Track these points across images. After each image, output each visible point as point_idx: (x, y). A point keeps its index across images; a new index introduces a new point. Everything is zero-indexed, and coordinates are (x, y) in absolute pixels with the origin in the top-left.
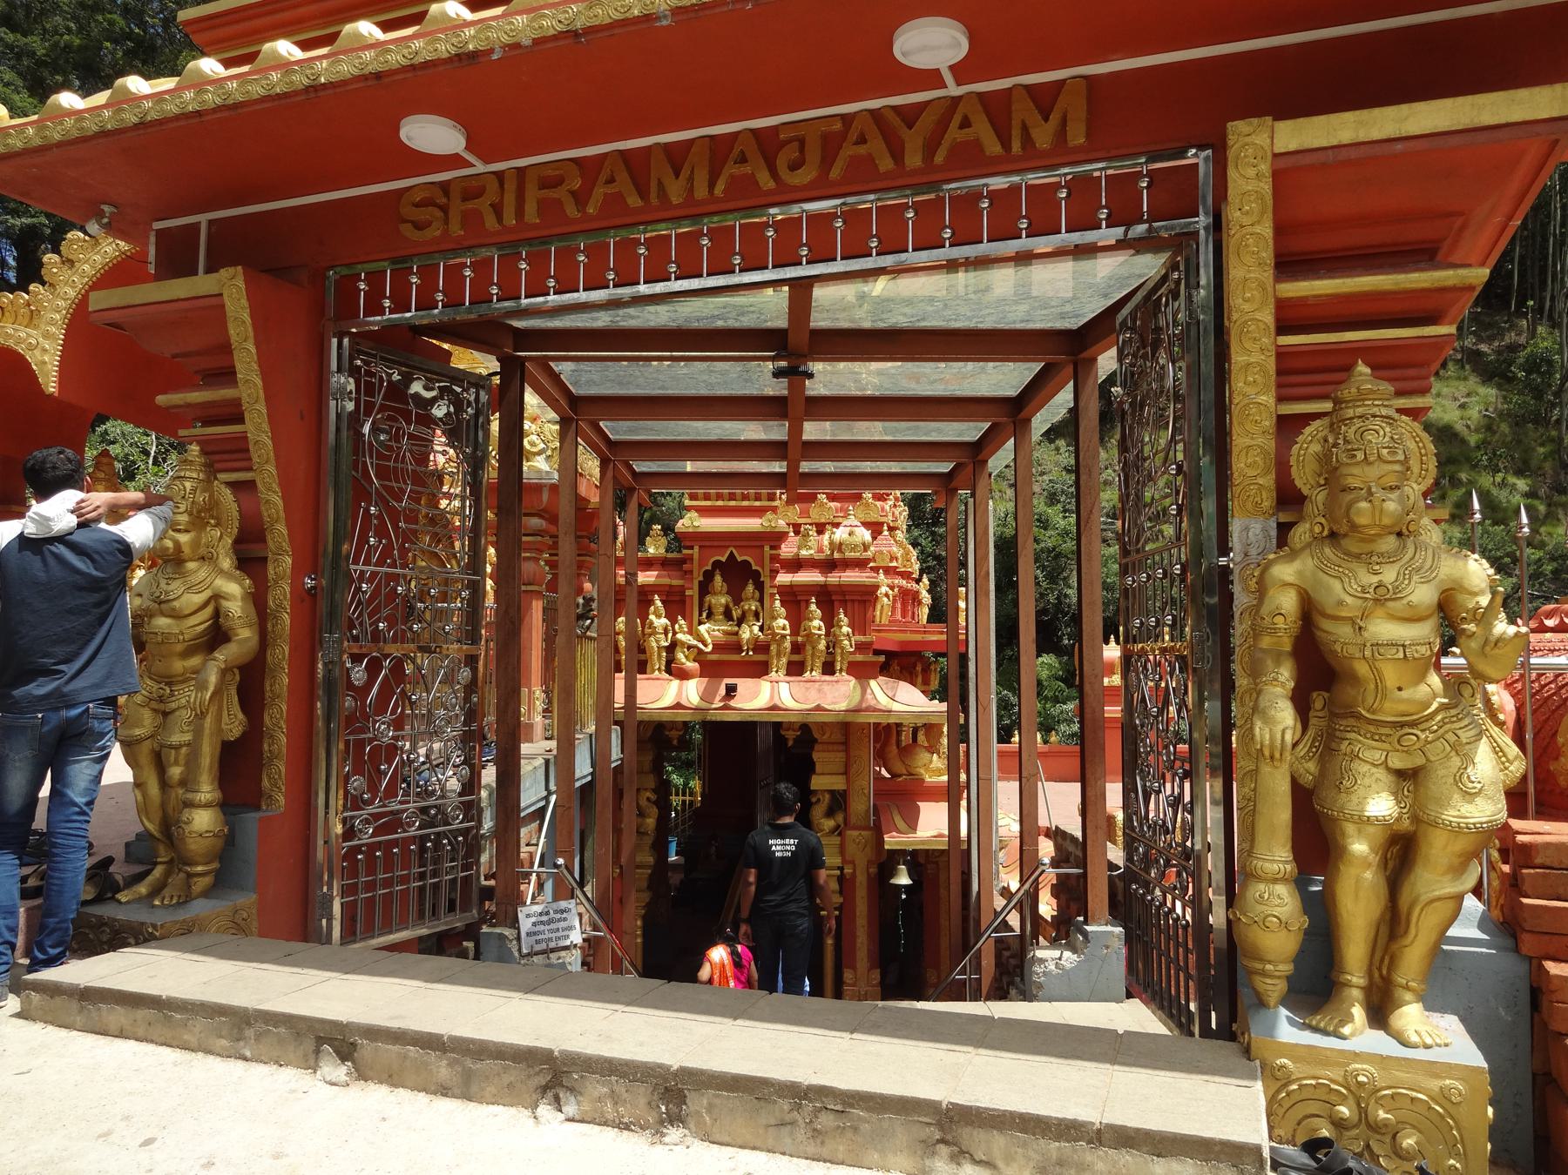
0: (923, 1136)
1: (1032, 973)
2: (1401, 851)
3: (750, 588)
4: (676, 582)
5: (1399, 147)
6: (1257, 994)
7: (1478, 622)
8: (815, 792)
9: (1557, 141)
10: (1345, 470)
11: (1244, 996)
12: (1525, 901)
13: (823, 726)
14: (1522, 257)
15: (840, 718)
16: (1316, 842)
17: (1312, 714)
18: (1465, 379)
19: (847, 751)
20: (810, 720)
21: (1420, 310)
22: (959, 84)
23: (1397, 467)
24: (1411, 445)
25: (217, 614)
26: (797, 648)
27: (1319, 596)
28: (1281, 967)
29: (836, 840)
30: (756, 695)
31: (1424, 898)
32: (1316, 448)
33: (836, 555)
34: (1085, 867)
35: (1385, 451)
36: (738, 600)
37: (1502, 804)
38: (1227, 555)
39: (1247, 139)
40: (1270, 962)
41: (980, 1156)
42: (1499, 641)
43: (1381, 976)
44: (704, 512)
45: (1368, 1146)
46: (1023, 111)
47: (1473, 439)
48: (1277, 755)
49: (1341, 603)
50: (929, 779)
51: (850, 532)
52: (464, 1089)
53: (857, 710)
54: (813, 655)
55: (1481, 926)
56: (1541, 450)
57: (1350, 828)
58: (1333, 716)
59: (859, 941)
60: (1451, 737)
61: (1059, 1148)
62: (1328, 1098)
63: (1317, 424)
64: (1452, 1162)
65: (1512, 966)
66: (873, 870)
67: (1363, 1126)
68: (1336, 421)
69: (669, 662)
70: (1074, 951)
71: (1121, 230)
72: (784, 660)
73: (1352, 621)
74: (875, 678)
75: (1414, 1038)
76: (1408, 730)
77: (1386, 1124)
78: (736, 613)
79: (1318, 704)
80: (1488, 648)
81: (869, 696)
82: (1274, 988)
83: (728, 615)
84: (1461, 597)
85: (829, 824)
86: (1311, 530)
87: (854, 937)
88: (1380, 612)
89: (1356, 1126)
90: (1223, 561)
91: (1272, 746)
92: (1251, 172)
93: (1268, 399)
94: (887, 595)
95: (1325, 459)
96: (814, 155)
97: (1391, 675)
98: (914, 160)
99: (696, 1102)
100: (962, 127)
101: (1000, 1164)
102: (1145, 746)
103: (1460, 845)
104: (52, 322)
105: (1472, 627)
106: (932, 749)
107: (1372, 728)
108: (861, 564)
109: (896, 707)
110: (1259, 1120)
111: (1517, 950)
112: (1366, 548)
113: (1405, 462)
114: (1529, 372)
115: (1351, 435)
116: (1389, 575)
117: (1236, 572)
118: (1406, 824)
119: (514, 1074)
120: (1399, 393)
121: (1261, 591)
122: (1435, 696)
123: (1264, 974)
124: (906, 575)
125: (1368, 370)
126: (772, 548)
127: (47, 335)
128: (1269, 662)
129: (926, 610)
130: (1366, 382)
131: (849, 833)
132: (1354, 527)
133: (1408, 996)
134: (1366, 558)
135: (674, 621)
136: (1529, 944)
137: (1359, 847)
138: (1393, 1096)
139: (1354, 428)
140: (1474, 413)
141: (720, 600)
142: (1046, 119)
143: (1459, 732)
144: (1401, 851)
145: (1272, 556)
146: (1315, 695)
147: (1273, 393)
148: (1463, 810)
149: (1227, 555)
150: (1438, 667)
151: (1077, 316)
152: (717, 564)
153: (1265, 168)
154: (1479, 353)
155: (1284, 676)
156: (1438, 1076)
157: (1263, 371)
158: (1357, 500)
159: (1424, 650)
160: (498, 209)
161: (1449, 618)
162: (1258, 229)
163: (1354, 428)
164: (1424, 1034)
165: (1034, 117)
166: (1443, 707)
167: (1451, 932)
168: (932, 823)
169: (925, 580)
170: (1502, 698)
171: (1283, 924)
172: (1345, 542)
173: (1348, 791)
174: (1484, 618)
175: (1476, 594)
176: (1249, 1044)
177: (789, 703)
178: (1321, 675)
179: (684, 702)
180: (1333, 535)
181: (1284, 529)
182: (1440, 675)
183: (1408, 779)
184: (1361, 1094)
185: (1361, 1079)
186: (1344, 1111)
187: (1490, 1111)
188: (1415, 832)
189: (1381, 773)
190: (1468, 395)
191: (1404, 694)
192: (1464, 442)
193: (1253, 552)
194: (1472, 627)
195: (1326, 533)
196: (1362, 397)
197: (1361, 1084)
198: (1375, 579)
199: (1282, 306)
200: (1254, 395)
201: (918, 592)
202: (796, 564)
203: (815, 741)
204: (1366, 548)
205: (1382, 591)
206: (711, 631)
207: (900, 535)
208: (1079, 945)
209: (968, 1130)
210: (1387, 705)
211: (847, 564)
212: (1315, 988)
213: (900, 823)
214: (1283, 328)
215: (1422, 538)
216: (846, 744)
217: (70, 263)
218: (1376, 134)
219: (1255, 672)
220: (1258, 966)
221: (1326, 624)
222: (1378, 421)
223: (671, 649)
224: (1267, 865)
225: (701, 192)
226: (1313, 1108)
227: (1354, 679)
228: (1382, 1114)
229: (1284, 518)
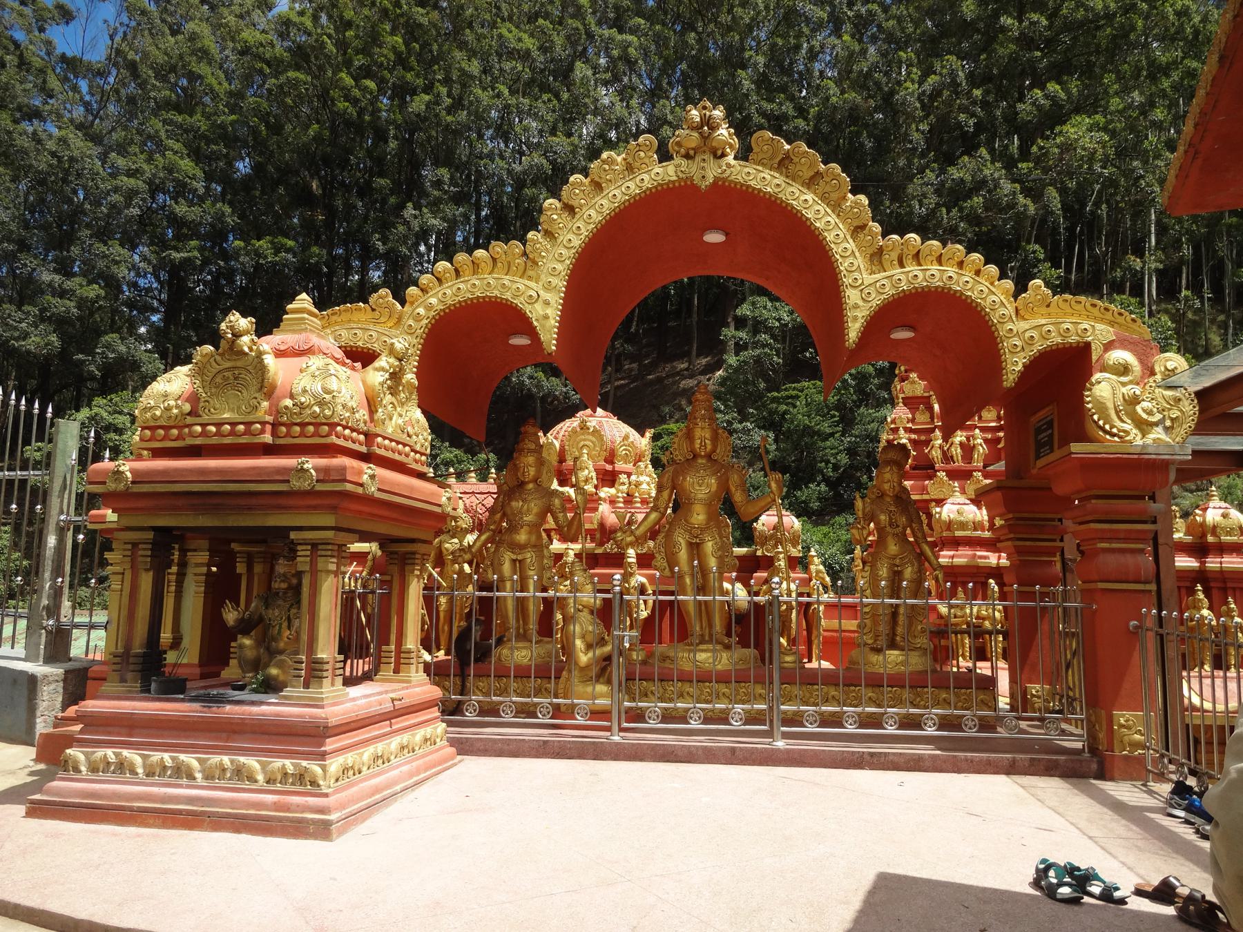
127: (548, 287)
217: (570, 209)
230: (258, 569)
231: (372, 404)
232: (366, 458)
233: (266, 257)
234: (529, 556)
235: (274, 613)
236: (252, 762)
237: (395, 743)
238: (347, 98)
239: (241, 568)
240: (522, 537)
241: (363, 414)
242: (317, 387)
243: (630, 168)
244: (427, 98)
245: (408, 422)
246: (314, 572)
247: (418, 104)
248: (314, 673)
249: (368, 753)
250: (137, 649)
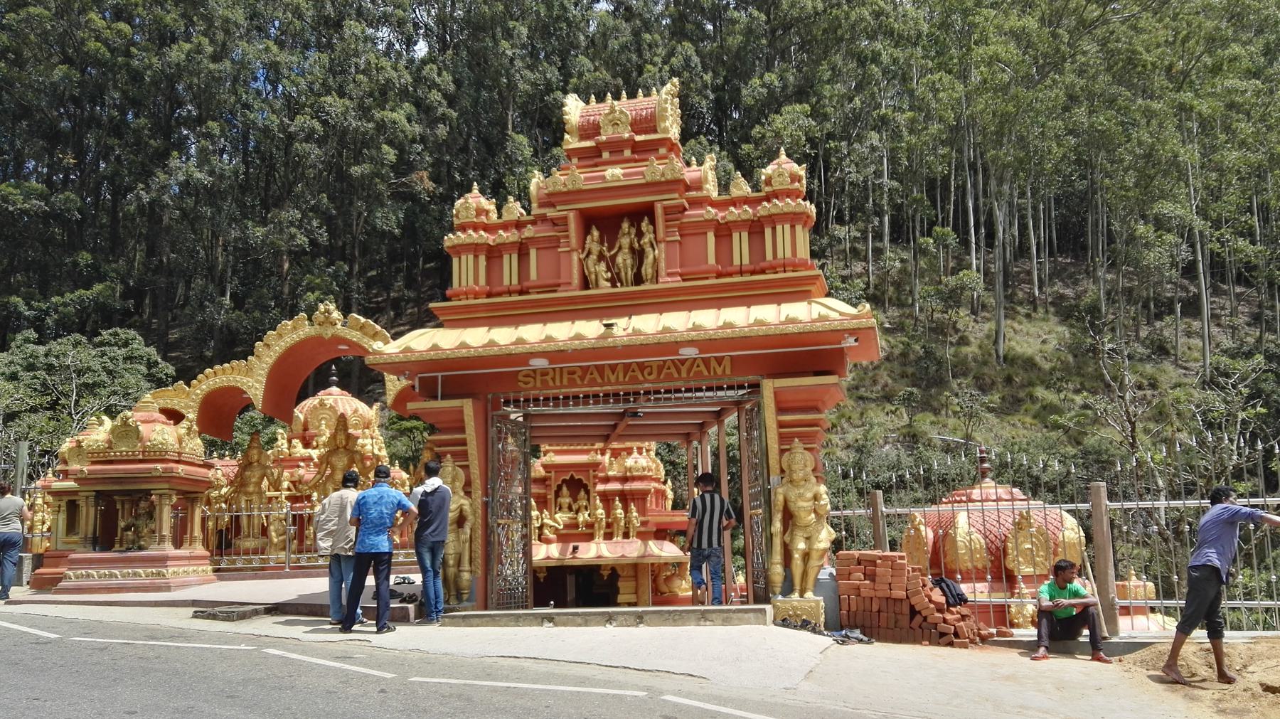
2: (806, 556)
3: (582, 493)
4: (542, 491)
13: (623, 566)
19: (636, 580)
25: (461, 511)
26: (609, 525)
30: (588, 551)
36: (575, 500)
44: (557, 452)
46: (714, 363)
50: (682, 594)
52: (586, 624)
53: (643, 557)
69: (540, 536)
78: (575, 507)
82: (778, 590)
83: (570, 509)
96: (655, 372)
97: (803, 514)
98: (684, 375)
99: (646, 618)
104: (260, 375)
109: (663, 554)
119: (599, 618)
124: (657, 480)
127: (257, 381)
135: (542, 513)
137: (797, 556)
140: (1053, 344)
141: (565, 500)
144: (806, 556)
152: (564, 481)
160: (553, 379)
169: (669, 482)
177: (606, 553)
178: (789, 517)
183: (808, 539)
206: (562, 518)
211: (634, 479)
212: (788, 589)
216: (636, 577)
217: (268, 346)
223: (541, 528)
225: (621, 379)
230: (127, 506)
231: (180, 441)
232: (178, 462)
233: (14, 204)
234: (255, 498)
235: (140, 523)
236: (140, 571)
237: (191, 569)
238: (97, 39)
239: (119, 506)
240: (251, 489)
241: (177, 446)
242: (160, 439)
243: (295, 328)
244: (187, 46)
245: (196, 445)
246: (161, 505)
247: (176, 53)
248: (162, 540)
249: (181, 569)
250: (90, 535)
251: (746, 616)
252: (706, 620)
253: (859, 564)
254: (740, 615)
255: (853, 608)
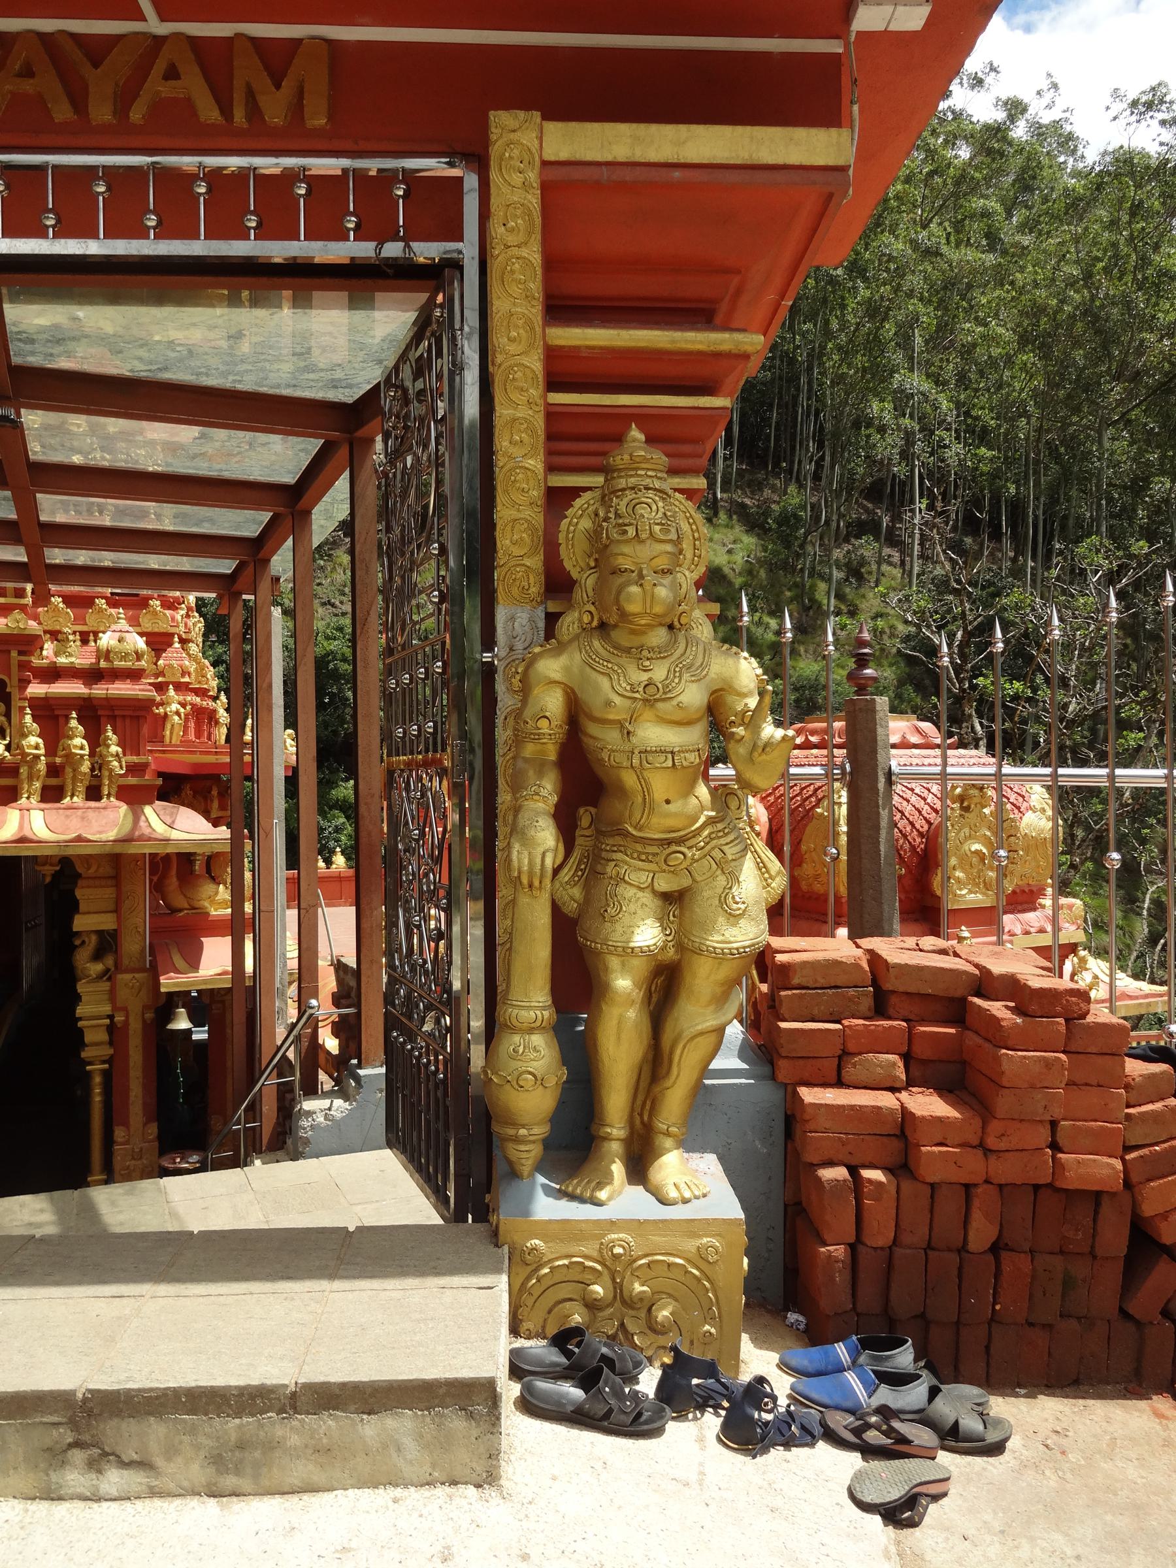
0: (48, 1442)
1: (298, 1127)
2: (665, 982)
5: (677, 174)
6: (510, 1163)
7: (747, 726)
8: (78, 933)
9: (830, 196)
10: (615, 549)
11: (499, 1168)
12: (783, 1025)
13: (87, 859)
14: (777, 423)
15: (107, 850)
16: (577, 979)
17: (578, 833)
18: (732, 527)
19: (118, 886)
20: (70, 852)
21: (694, 377)
22: (163, 19)
23: (669, 548)
24: (685, 527)
26: (54, 770)
27: (594, 703)
28: (536, 1131)
29: (105, 986)
31: (687, 1034)
32: (586, 524)
33: (103, 664)
34: (358, 1005)
35: (657, 528)
37: (765, 925)
38: (491, 650)
39: (512, 136)
40: (523, 1126)
41: (131, 1455)
42: (768, 745)
43: (642, 1122)
45: (622, 1325)
46: (247, 70)
47: (738, 581)
48: (536, 883)
49: (609, 703)
51: (120, 636)
53: (127, 840)
54: (74, 779)
55: (742, 1056)
56: (788, 594)
57: (614, 962)
58: (600, 834)
59: (132, 1094)
60: (717, 854)
61: (240, 1427)
62: (580, 1277)
63: (587, 496)
64: (707, 1327)
65: (769, 1094)
66: (149, 1016)
67: (618, 1304)
68: (607, 496)
70: (346, 1098)
71: (371, 245)
72: (37, 785)
73: (620, 724)
74: (150, 803)
75: (673, 1194)
76: (674, 848)
77: (641, 1297)
79: (585, 821)
80: (756, 754)
81: (142, 823)
82: (527, 1153)
84: (730, 699)
85: (96, 968)
86: (580, 620)
87: (127, 1090)
88: (648, 714)
89: (610, 1305)
90: (487, 657)
91: (531, 874)
92: (517, 179)
93: (536, 464)
94: (178, 713)
95: (594, 536)
97: (660, 785)
100: (167, 77)
101: (159, 1462)
102: (407, 875)
103: (725, 972)
105: (740, 731)
106: (216, 880)
107: (639, 847)
108: (134, 675)
109: (175, 835)
110: (496, 1338)
111: (773, 1078)
112: (636, 641)
113: (678, 542)
114: (780, 525)
115: (622, 508)
116: (659, 673)
117: (500, 669)
118: (671, 953)
120: (673, 471)
121: (525, 690)
122: (703, 808)
123: (517, 1140)
124: (202, 692)
125: (642, 437)
126: (20, 653)
128: (531, 773)
129: (224, 730)
130: (640, 448)
131: (120, 976)
132: (624, 615)
133: (668, 1143)
134: (637, 654)
136: (785, 1070)
137: (623, 983)
138: (649, 1265)
139: (626, 500)
140: (739, 558)
142: (278, 86)
143: (725, 848)
144: (665, 982)
145: (537, 650)
146: (582, 810)
147: (541, 457)
148: (727, 934)
149: (491, 650)
150: (706, 777)
151: (350, 386)
153: (533, 176)
154: (743, 506)
155: (545, 792)
156: (695, 1235)
157: (532, 431)
158: (628, 583)
159: (693, 758)
161: (716, 717)
162: (524, 252)
163: (626, 500)
164: (682, 1186)
165: (263, 82)
166: (711, 821)
167: (715, 1065)
168: (215, 960)
170: (758, 810)
171: (539, 1081)
172: (615, 634)
173: (613, 920)
174: (752, 721)
175: (745, 695)
176: (497, 1226)
178: (588, 789)
179: (28, 834)
180: (603, 626)
181: (552, 619)
182: (708, 787)
183: (674, 901)
184: (616, 1268)
185: (618, 1250)
186: (598, 1289)
187: (746, 1260)
188: (680, 961)
189: (646, 898)
190: (735, 542)
191: (672, 807)
192: (730, 583)
193: (519, 646)
194: (740, 731)
195: (595, 623)
196: (633, 467)
197: (616, 1257)
198: (644, 677)
199: (552, 355)
200: (522, 461)
201: (215, 711)
202: (53, 674)
203: (79, 876)
204: (636, 641)
205: (651, 690)
207: (194, 648)
208: (351, 1091)
209: (114, 1422)
210: (654, 820)
211: (116, 675)
212: (574, 1148)
213: (178, 961)
214: (554, 383)
215: (694, 632)
218: (653, 156)
219: (516, 787)
220: (511, 1132)
221: (593, 729)
222: (651, 494)
224: (523, 1013)
226: (564, 1291)
227: (621, 792)
228: (638, 1288)
229: (552, 607)
251: (371, 1428)
252: (102, 1458)
253: (880, 1008)
254: (329, 1424)
255: (880, 1234)
